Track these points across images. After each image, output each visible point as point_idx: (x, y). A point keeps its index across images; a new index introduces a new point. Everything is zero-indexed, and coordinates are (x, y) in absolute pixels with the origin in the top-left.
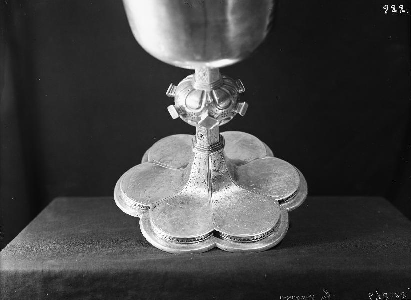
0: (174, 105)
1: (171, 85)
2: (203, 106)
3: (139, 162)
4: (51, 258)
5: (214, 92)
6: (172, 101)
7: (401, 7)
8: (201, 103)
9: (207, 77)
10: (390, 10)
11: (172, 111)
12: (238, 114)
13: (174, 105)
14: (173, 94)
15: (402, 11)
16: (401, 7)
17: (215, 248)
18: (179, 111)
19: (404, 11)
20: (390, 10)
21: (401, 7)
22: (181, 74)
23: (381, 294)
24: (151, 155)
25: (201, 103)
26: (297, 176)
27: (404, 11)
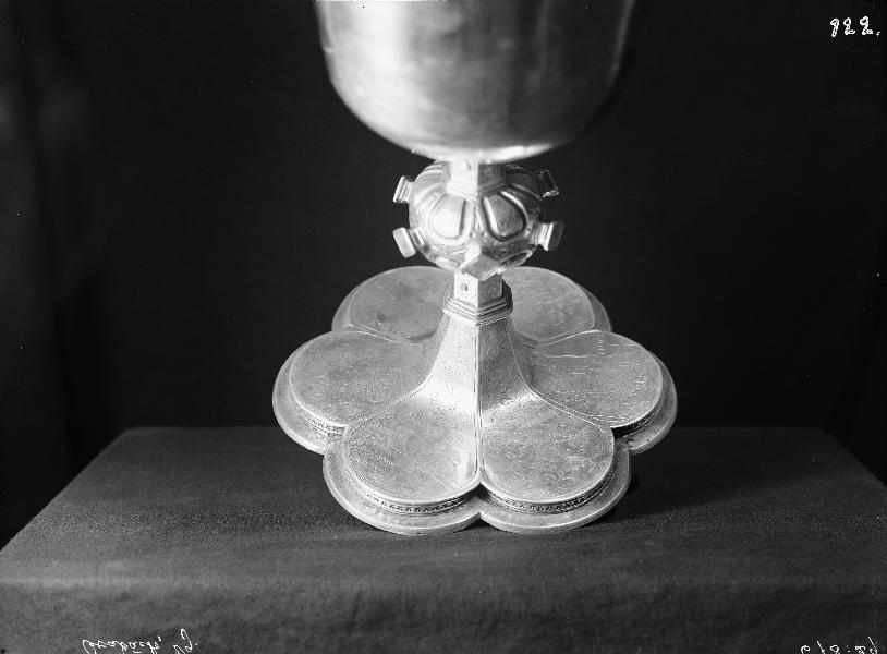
0: (407, 226)
1: (403, 178)
2: (467, 230)
3: (328, 329)
4: (115, 557)
5: (487, 201)
6: (401, 215)
7: (865, 22)
8: (462, 226)
9: (476, 485)
10: (857, 26)
11: (401, 237)
12: (540, 247)
13: (407, 226)
14: (406, 199)
15: (867, 31)
16: (847, 22)
17: (478, 523)
18: (414, 240)
19: (871, 32)
20: (842, 28)
21: (847, 22)
22: (414, 164)
23: (826, 647)
24: (349, 317)
25: (462, 226)
26: (660, 381)
27: (871, 32)
